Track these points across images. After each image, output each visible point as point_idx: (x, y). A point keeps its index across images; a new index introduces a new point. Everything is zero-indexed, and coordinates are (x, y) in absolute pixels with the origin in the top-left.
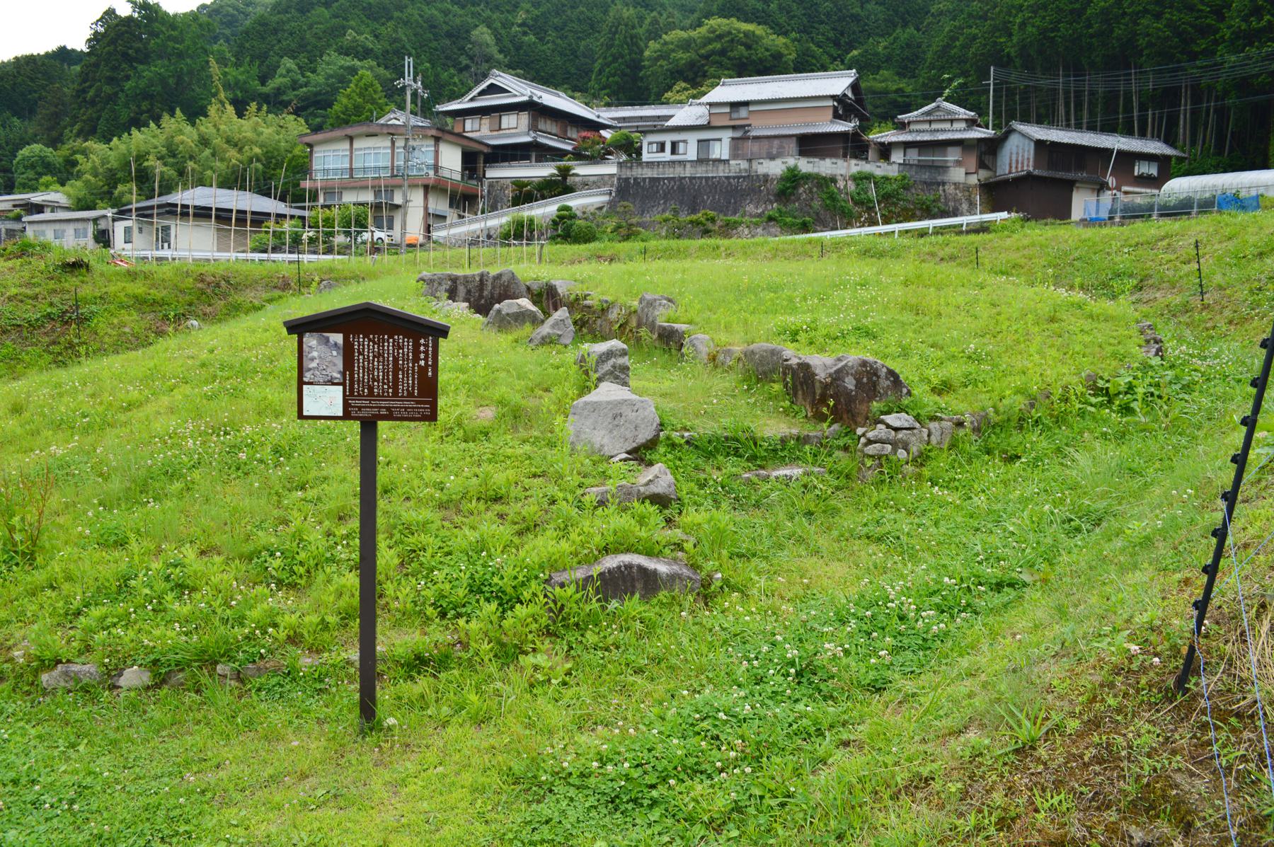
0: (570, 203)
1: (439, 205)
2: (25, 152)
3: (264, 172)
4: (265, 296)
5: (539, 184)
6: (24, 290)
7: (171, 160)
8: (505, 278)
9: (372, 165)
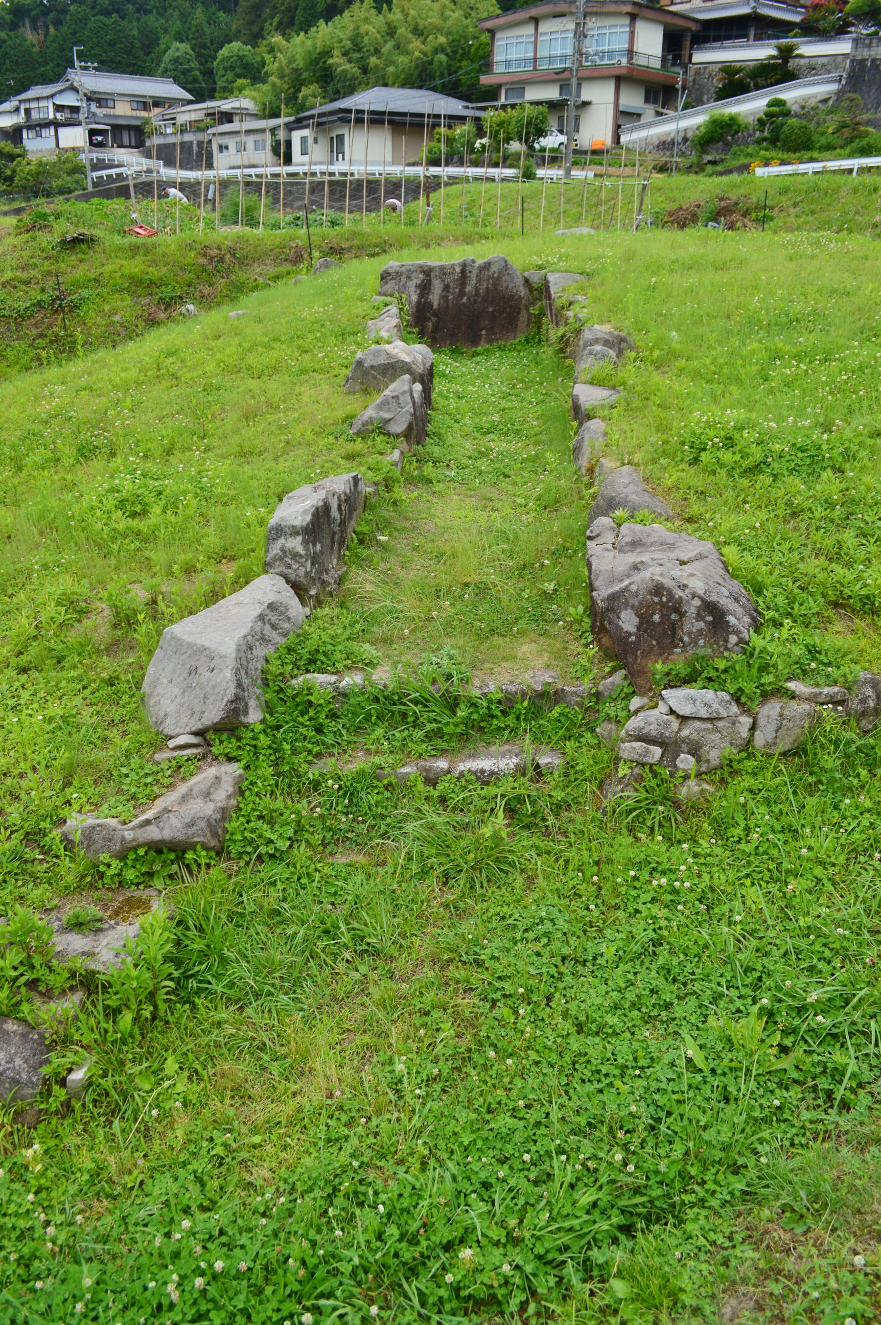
0: (784, 96)
1: (633, 100)
2: (224, 52)
3: (449, 65)
4: (273, 271)
5: (756, 68)
6: (19, 274)
7: (356, 55)
8: (494, 268)
9: (559, 52)
